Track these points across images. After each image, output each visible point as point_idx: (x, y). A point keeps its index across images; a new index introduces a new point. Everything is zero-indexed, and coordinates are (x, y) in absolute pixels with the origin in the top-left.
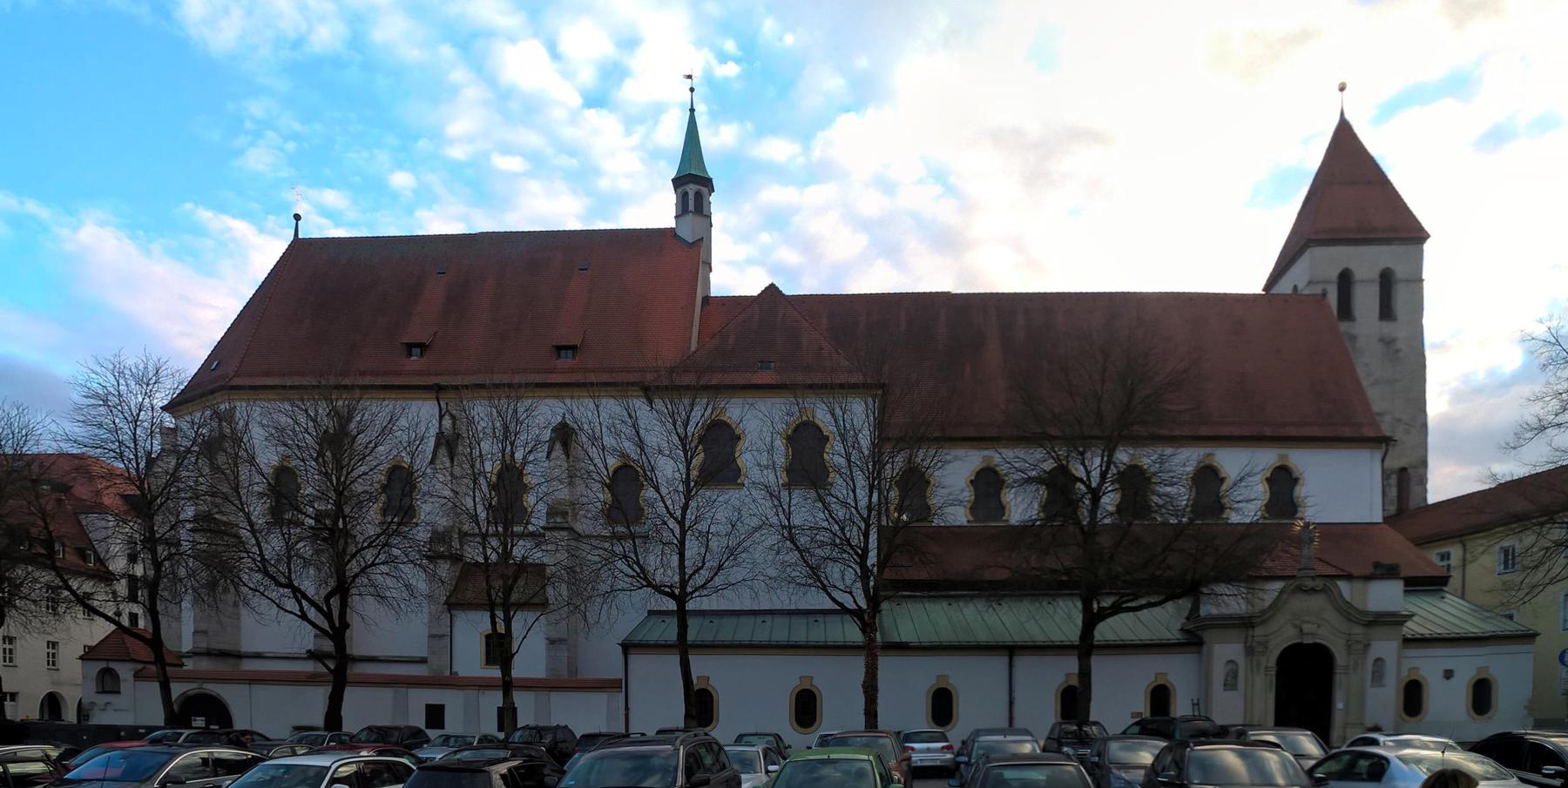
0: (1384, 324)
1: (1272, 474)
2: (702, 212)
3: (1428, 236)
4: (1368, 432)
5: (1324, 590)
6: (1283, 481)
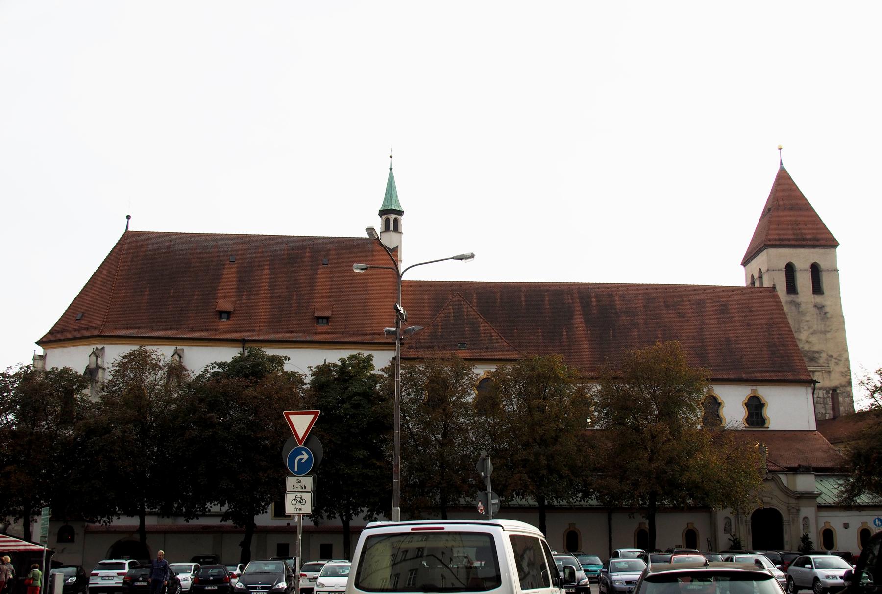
0: (816, 296)
1: (748, 401)
2: (397, 230)
3: (839, 244)
4: (803, 377)
5: (773, 479)
6: (755, 407)
